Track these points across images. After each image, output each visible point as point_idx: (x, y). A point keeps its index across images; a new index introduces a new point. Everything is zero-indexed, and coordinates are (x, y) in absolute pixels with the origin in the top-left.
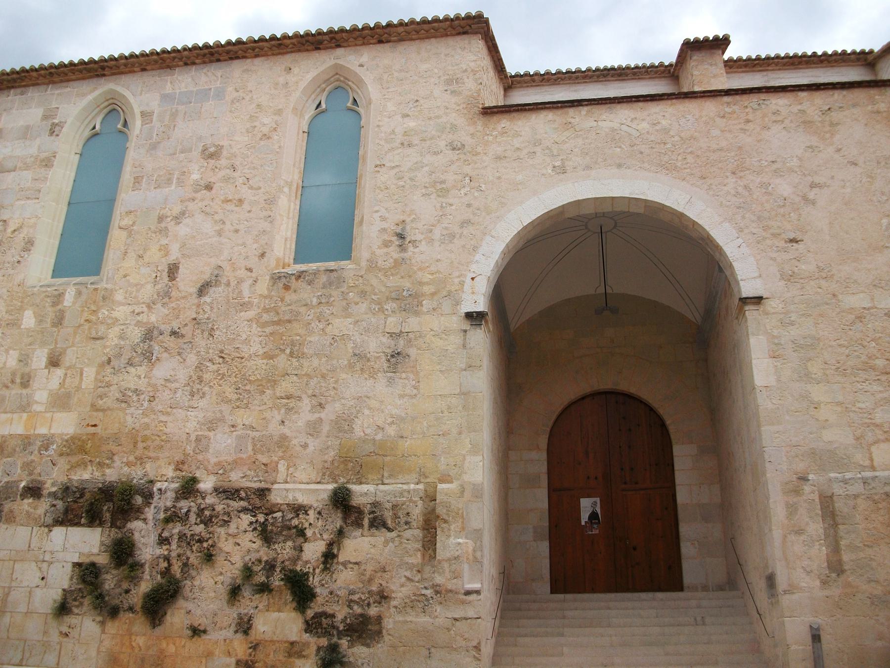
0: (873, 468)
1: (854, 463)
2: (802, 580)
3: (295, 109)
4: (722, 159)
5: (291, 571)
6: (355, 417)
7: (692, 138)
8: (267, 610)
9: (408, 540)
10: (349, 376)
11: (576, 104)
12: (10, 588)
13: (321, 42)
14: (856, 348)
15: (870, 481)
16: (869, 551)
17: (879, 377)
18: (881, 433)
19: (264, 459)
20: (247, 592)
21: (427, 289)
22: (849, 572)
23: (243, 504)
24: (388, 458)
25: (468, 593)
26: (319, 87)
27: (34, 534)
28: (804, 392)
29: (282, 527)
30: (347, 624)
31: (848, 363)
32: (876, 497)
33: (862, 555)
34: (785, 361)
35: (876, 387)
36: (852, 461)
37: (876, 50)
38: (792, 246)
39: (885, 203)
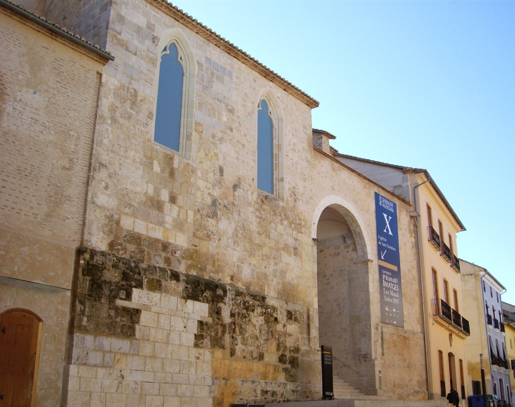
12: (170, 330)
13: (268, 75)
27: (179, 302)
37: (339, 152)
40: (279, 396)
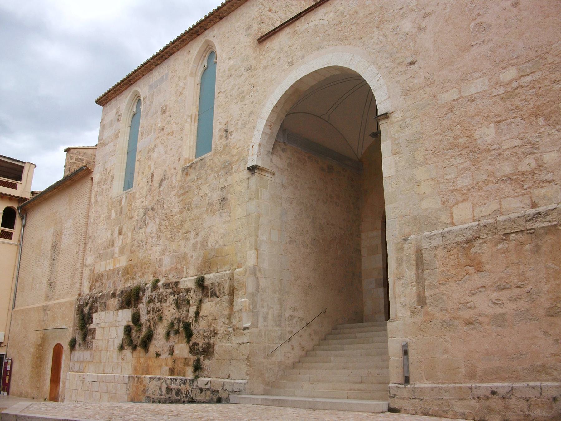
0: (453, 224)
1: (441, 222)
2: (400, 312)
3: (191, 73)
4: (371, 20)
5: (185, 322)
6: (209, 238)
7: (356, 12)
8: (178, 343)
9: (224, 302)
10: (207, 216)
11: (298, 17)
14: (447, 133)
15: (446, 235)
16: (442, 288)
17: (460, 152)
18: (460, 195)
19: (179, 266)
20: (172, 334)
21: (235, 158)
22: (429, 304)
23: (171, 290)
24: (220, 258)
25: (244, 329)
26: (202, 56)
28: (411, 175)
29: (182, 300)
30: (203, 348)
31: (441, 146)
32: (450, 247)
33: (437, 291)
34: (401, 155)
35: (459, 160)
36: (439, 221)
38: (411, 67)
39: (473, 9)
40: (184, 395)
